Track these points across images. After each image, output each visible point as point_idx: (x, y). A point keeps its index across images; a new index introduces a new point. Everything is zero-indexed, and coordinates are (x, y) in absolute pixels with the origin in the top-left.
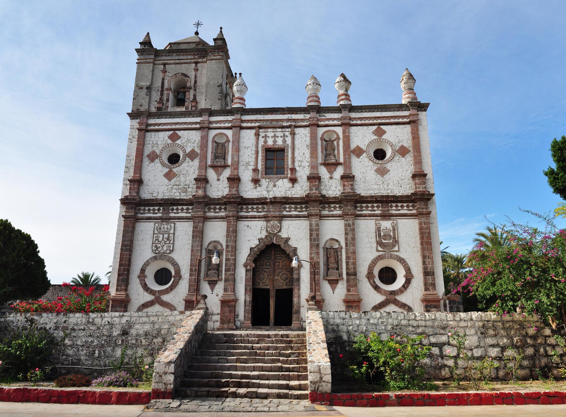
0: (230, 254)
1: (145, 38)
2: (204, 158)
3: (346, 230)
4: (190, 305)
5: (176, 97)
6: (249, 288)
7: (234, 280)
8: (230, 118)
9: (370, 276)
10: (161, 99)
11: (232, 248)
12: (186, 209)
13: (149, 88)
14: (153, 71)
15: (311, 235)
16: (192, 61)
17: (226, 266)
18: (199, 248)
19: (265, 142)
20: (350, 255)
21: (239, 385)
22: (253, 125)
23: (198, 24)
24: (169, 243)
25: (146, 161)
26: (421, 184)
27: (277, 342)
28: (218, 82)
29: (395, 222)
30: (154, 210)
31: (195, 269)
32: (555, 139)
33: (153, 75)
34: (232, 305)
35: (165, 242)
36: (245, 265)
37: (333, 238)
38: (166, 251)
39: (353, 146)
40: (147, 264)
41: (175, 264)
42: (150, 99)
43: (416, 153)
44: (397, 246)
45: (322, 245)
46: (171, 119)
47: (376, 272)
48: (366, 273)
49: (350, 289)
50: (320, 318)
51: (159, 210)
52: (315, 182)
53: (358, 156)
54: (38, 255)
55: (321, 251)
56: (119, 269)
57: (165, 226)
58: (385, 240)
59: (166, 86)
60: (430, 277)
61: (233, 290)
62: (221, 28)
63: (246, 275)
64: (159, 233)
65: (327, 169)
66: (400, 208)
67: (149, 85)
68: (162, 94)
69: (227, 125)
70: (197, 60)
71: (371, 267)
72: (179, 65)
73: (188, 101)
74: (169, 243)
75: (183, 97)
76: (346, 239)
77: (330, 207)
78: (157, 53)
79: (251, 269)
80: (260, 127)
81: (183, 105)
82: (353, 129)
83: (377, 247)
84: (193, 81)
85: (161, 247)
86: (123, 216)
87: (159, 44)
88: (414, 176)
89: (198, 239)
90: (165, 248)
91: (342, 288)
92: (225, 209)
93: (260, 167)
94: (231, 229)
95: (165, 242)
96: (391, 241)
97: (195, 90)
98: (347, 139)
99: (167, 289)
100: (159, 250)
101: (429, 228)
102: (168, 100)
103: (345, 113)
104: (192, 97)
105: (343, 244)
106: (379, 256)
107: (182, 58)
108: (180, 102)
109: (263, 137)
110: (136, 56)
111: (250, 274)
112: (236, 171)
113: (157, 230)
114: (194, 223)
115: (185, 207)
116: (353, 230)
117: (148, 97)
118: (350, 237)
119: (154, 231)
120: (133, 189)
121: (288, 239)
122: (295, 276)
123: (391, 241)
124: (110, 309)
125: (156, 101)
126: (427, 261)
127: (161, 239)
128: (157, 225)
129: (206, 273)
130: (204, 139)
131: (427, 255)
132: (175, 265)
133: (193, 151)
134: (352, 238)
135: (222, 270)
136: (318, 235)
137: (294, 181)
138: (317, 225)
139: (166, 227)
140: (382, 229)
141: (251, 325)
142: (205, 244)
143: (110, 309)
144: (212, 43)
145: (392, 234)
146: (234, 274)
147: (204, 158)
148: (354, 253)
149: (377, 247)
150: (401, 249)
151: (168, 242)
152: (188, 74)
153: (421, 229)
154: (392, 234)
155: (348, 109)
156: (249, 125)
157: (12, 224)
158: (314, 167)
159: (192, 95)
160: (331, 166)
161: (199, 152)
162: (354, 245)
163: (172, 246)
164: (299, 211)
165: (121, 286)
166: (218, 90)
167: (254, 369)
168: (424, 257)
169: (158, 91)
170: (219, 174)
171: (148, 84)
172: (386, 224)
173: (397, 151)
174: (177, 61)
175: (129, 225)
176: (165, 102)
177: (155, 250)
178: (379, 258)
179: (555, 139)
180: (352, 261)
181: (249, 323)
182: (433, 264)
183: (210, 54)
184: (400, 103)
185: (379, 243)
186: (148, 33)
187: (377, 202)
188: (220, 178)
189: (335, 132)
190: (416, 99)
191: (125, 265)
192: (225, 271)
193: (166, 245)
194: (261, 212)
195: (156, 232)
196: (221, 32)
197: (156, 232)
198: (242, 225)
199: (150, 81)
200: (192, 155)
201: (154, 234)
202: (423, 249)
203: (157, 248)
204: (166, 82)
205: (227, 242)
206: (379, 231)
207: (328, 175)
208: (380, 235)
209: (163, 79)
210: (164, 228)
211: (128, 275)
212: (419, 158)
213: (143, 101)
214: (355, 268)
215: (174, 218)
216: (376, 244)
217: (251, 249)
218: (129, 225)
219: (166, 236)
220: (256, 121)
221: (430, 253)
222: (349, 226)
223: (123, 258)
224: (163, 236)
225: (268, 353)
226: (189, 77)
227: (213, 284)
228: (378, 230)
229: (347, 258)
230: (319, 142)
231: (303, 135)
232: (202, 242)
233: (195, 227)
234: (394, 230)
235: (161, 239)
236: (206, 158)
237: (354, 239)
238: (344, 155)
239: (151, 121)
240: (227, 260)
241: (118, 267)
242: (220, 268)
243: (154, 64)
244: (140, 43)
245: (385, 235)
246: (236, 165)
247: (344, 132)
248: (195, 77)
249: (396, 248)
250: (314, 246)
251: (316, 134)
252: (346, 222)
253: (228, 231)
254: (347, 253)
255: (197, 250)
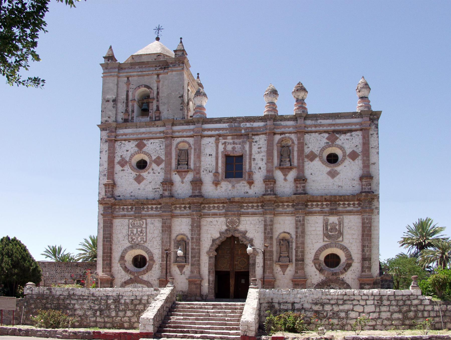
0: (194, 244)
1: (109, 51)
2: (169, 163)
3: (297, 224)
4: (163, 283)
5: (140, 106)
6: (221, 239)
7: (199, 265)
8: (192, 127)
9: (316, 259)
10: (127, 111)
11: (196, 240)
12: (155, 208)
13: (114, 101)
14: (117, 84)
15: (265, 229)
16: (154, 72)
17: (192, 254)
18: (168, 240)
19: (225, 148)
20: (299, 245)
21: (196, 332)
22: (213, 133)
23: (159, 29)
24: (142, 236)
25: (118, 168)
26: (367, 185)
27: (226, 308)
28: (179, 93)
29: (341, 217)
30: (322, 205)
31: (166, 254)
32: (101, 65)
33: (118, 87)
34: (198, 284)
35: (139, 234)
36: (208, 253)
37: (285, 231)
38: (140, 242)
39: (307, 151)
40: (125, 251)
41: (344, 249)
42: (116, 110)
43: (365, 158)
44: (341, 237)
45: (276, 235)
46: (345, 120)
47: (322, 257)
48: (313, 258)
49: (297, 272)
50: (35, 52)
51: (132, 209)
52: (270, 184)
53: (312, 160)
54: (310, 114)
55: (275, 242)
56: (103, 256)
57: (137, 222)
58: (331, 232)
59: (130, 97)
60: (367, 262)
61: (198, 272)
62: (181, 38)
63: (209, 261)
64: (134, 227)
65: (282, 172)
66: (346, 206)
67: (115, 98)
68: (127, 106)
69: (189, 134)
70: (158, 72)
71: (317, 255)
72: (141, 77)
73: (151, 111)
74: (142, 236)
75: (146, 107)
76: (297, 232)
77: (283, 205)
78: (120, 67)
79: (213, 257)
80: (219, 135)
81: (148, 115)
82: (307, 136)
83: (324, 238)
84: (155, 93)
85: (136, 239)
86: (105, 185)
87: (121, 58)
88: (361, 178)
89: (167, 233)
90: (139, 239)
91: (291, 270)
92: (190, 208)
93: (220, 170)
94: (195, 225)
95: (139, 234)
96: (337, 233)
97: (158, 101)
98: (302, 145)
99: (144, 271)
100: (135, 241)
101: (370, 223)
102: (133, 111)
103: (300, 121)
104: (155, 108)
105: (294, 236)
106: (325, 245)
107: (144, 70)
108: (145, 111)
109: (223, 144)
110: (101, 70)
111: (213, 260)
112: (198, 175)
113: (132, 225)
114: (163, 219)
115: (154, 206)
116: (303, 225)
117: (115, 109)
118: (300, 230)
119: (129, 226)
120: (108, 191)
121: (245, 232)
122: (251, 262)
123: (337, 233)
124: (99, 285)
125: (122, 112)
126: (366, 249)
127: (135, 232)
128: (131, 221)
129: (175, 259)
130: (168, 147)
131: (367, 244)
132: (149, 253)
133: (159, 158)
134: (302, 231)
135: (189, 257)
136: (272, 229)
137: (251, 183)
138: (272, 221)
139: (138, 222)
140: (329, 224)
141: (214, 298)
142: (174, 236)
143: (99, 285)
144: (173, 55)
145: (337, 227)
146: (199, 260)
147: (169, 163)
148: (303, 243)
149: (324, 238)
150: (344, 240)
151: (142, 234)
152: (151, 86)
153: (363, 223)
154: (337, 227)
155: (303, 118)
156: (210, 133)
157: (21, 242)
158: (269, 171)
159: (155, 106)
160: (285, 170)
161: (164, 159)
162: (303, 237)
163: (145, 237)
164: (255, 209)
165: (106, 269)
166: (180, 101)
167: (207, 324)
168: (363, 246)
169: (123, 102)
170: (183, 178)
171: (114, 97)
172: (333, 219)
173: (318, 156)
174: (140, 73)
175: (108, 222)
176: (130, 113)
177: (131, 241)
178: (325, 247)
179: (101, 65)
180: (300, 250)
181: (212, 296)
182: (370, 251)
183: (171, 66)
184: (355, 111)
185: (326, 235)
186: (111, 47)
187: (326, 200)
188: (184, 181)
189: (291, 139)
190: (369, 107)
191: (107, 253)
192: (192, 258)
193: (140, 237)
194: (222, 210)
195: (130, 226)
196: (181, 42)
197: (130, 226)
198: (205, 222)
199: (116, 94)
200: (158, 161)
201: (129, 228)
202: (363, 240)
203: (133, 240)
204: (130, 94)
205: (192, 235)
206: (326, 225)
207: (283, 177)
208: (327, 229)
209: (128, 92)
210: (137, 224)
211: (111, 260)
212: (368, 162)
213: (110, 113)
214: (303, 256)
215: (145, 216)
216: (323, 236)
217: (214, 241)
218: (108, 222)
219: (139, 230)
220: (216, 129)
221: (369, 243)
222: (300, 221)
223: (105, 247)
224: (137, 230)
225: (218, 315)
226: (152, 89)
227: (181, 268)
228: (326, 224)
229: (297, 247)
230: (275, 148)
231: (261, 140)
232: (170, 235)
233: (164, 223)
234: (340, 224)
235: (135, 232)
236: (170, 164)
237: (303, 232)
238: (298, 160)
239: (176, 128)
240: (193, 249)
241: (102, 255)
242: (187, 256)
243: (118, 77)
244: (105, 58)
245: (331, 229)
246: (197, 171)
247: (299, 139)
248: (158, 89)
249: (341, 239)
250: (268, 238)
251: (273, 141)
252: (296, 219)
253: (192, 226)
254: (297, 244)
255: (166, 241)
